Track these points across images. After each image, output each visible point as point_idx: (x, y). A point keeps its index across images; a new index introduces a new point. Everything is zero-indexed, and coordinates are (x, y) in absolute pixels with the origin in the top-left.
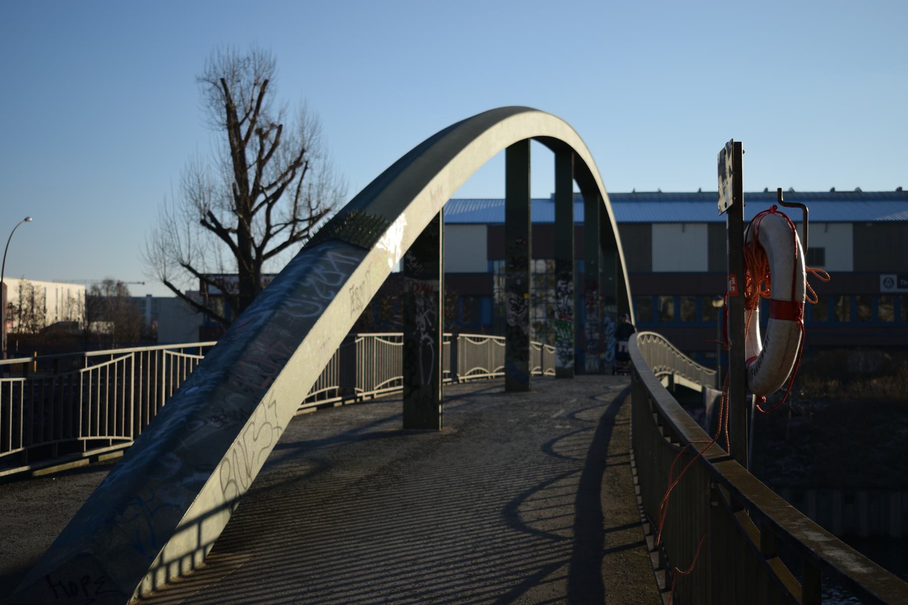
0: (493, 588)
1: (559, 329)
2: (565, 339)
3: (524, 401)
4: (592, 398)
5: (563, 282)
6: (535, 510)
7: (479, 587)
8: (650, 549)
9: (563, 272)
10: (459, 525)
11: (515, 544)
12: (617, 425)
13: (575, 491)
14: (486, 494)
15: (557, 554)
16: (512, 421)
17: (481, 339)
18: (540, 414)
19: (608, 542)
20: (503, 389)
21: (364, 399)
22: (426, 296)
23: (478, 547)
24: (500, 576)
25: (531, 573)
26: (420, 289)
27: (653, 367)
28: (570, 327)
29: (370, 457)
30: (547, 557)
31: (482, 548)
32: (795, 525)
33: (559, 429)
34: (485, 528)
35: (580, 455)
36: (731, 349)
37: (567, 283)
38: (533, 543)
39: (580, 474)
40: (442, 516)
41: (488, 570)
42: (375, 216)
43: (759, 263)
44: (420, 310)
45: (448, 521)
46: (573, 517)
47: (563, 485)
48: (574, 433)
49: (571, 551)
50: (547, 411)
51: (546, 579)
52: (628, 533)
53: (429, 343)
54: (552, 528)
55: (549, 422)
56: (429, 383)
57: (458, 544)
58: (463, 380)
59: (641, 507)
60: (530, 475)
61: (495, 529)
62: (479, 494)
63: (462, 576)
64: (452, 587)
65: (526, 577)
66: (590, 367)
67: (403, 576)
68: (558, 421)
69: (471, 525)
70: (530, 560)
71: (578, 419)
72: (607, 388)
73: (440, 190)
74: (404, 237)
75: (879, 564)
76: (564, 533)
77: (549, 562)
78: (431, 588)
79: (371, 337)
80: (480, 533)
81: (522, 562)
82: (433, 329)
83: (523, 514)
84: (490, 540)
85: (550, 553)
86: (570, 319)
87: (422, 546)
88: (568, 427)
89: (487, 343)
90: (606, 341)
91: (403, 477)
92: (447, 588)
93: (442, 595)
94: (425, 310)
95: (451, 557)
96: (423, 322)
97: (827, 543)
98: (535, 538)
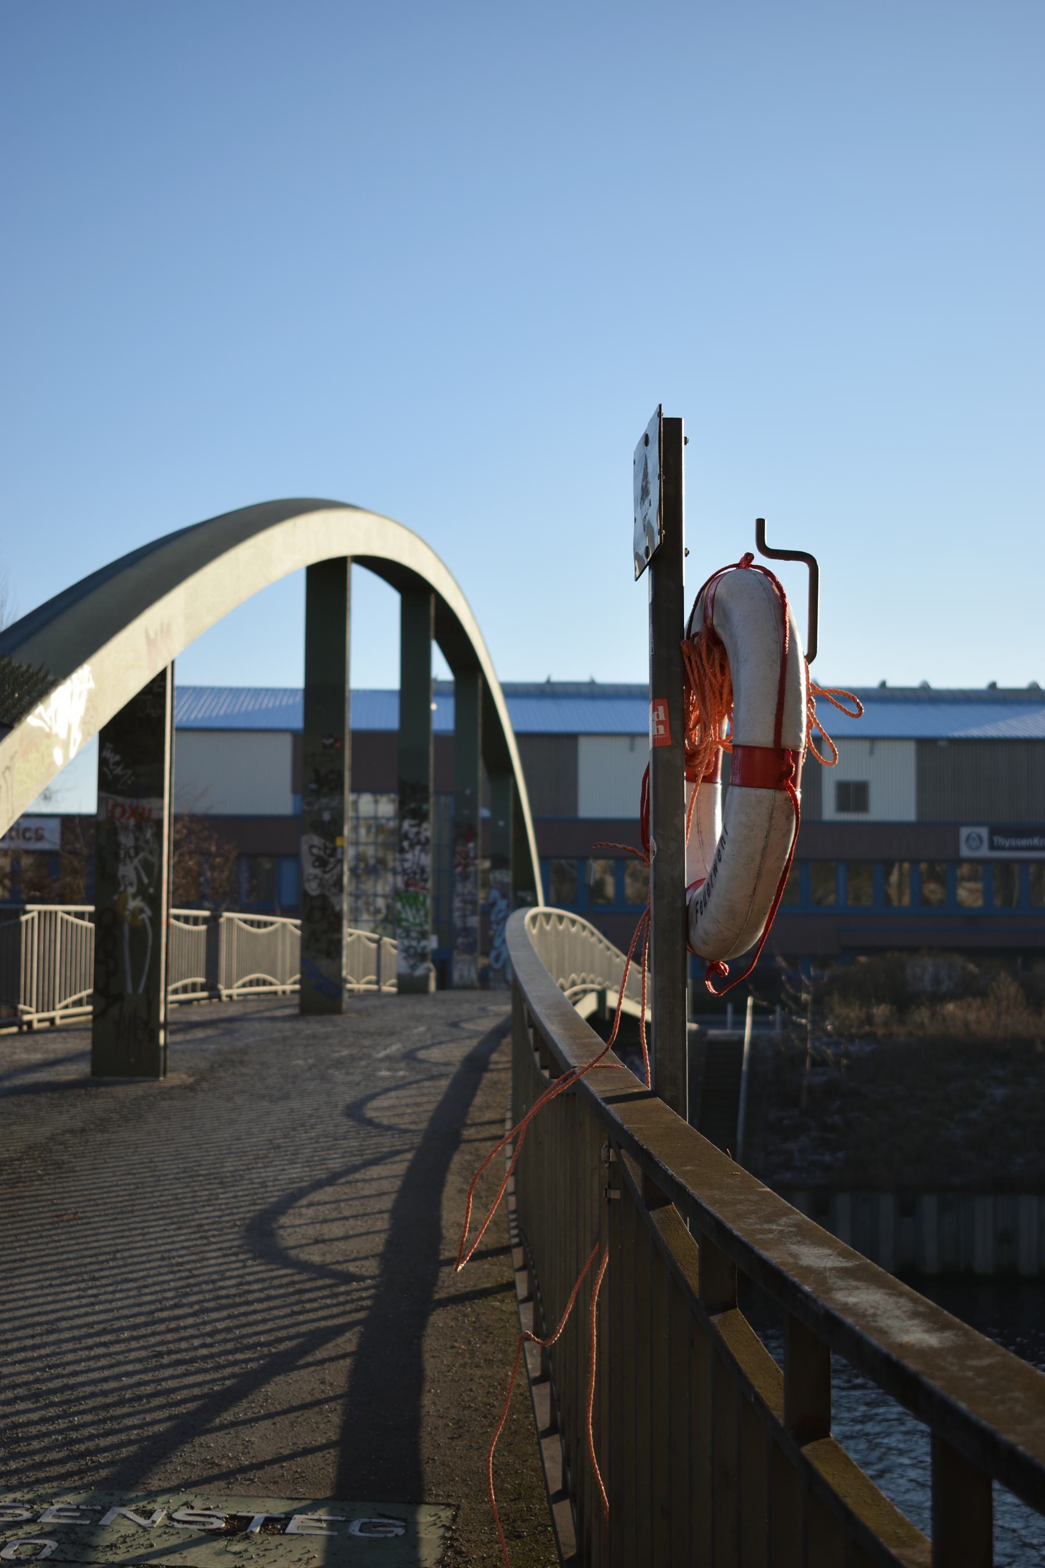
0: (200, 1378)
1: (403, 906)
2: (415, 925)
3: (330, 1029)
4: (455, 1025)
5: (413, 822)
6: (312, 1223)
7: (172, 1377)
8: (520, 1298)
9: (413, 805)
10: (157, 1252)
11: (261, 1290)
12: (492, 1071)
13: (396, 1188)
14: (223, 1193)
15: (341, 1308)
16: (300, 1062)
17: (266, 924)
18: (355, 1051)
19: (446, 1284)
20: (295, 1011)
21: (36, 1025)
22: (139, 828)
23: (187, 1295)
24: (220, 1354)
25: (282, 1347)
26: (127, 815)
27: (570, 974)
28: (424, 904)
29: (13, 1128)
30: (321, 1314)
31: (194, 1298)
32: (771, 1231)
33: (383, 1078)
34: (208, 1259)
35: (416, 1123)
36: (655, 860)
37: (419, 825)
38: (297, 1287)
39: (409, 1156)
40: (127, 1237)
41: (196, 1342)
42: (29, 667)
43: (715, 676)
44: (127, 853)
45: (139, 1245)
46: (384, 1236)
47: (375, 1176)
48: (410, 1083)
49: (369, 1303)
50: (368, 1047)
51: (309, 1359)
52: (486, 1266)
53: (143, 916)
54: (341, 1259)
55: (366, 1067)
56: (141, 990)
57: (147, 1290)
58: (230, 997)
59: (513, 1216)
60: (316, 1159)
61: (227, 1260)
62: (210, 1194)
63: (143, 1353)
64: (118, 1377)
65: (270, 1355)
66: (461, 977)
67: (21, 1356)
68: (386, 1064)
69: (182, 1252)
70: (287, 1322)
71: (422, 1061)
72: (484, 1009)
73: (166, 630)
74: (87, 709)
75: (970, 1324)
76: (362, 1266)
77: (323, 1324)
78: (72, 1381)
79: (51, 913)
80: (196, 1269)
81: (270, 1325)
82: (151, 890)
83: (289, 1230)
84: (214, 1282)
85: (328, 1307)
86: (424, 888)
87: (74, 1295)
88: (402, 1073)
89: (276, 931)
90: (491, 933)
91: (70, 1162)
92: (106, 1380)
93: (93, 1395)
94: (137, 854)
95: (127, 1317)
96: (132, 876)
97: (845, 1273)
98: (304, 1277)
